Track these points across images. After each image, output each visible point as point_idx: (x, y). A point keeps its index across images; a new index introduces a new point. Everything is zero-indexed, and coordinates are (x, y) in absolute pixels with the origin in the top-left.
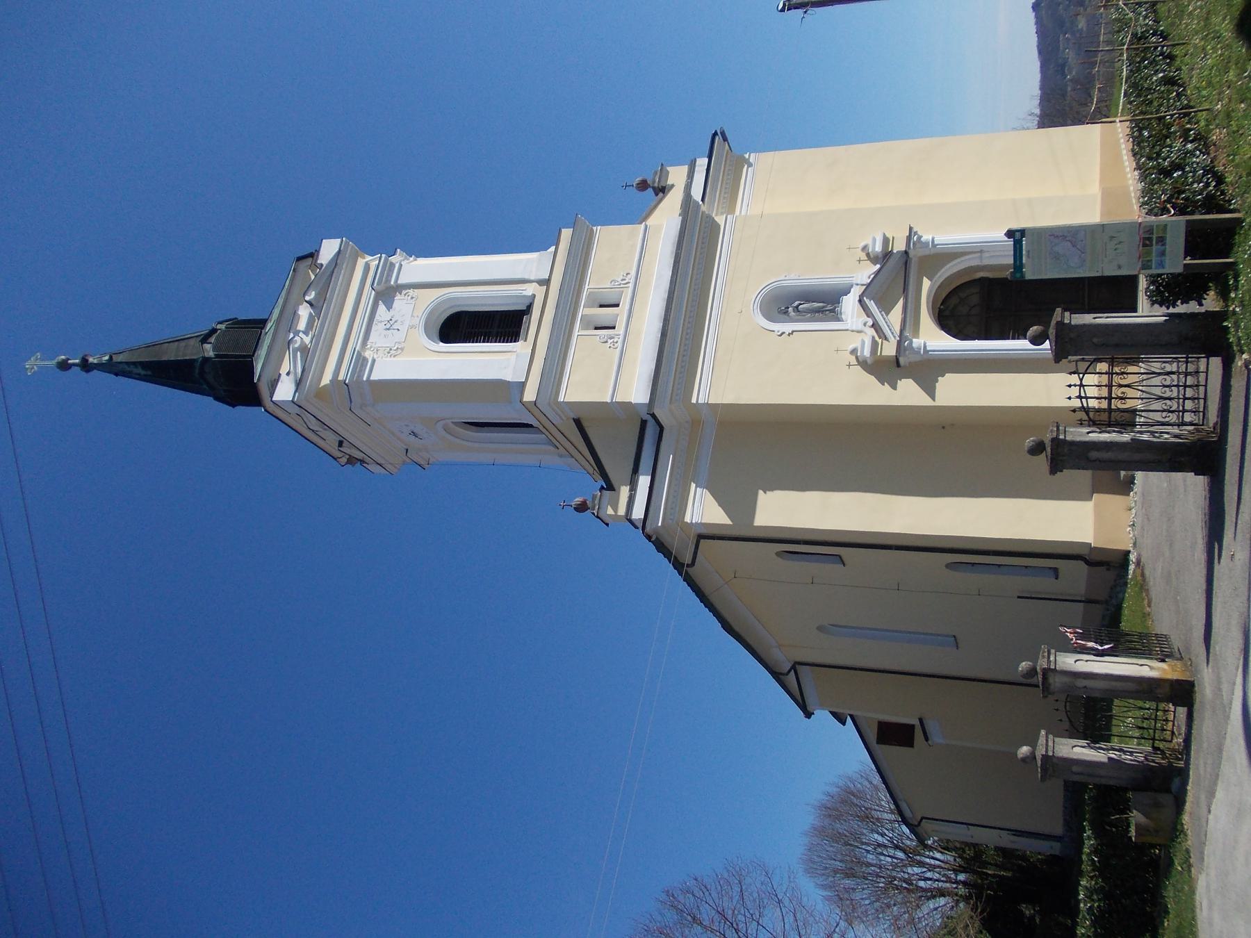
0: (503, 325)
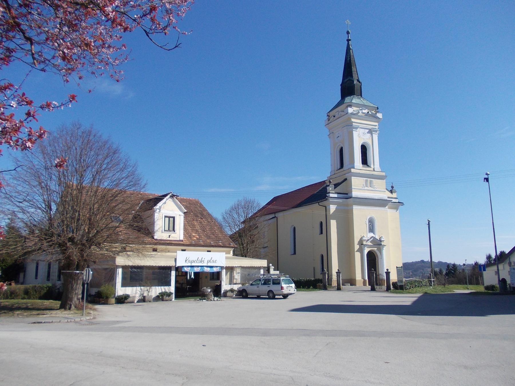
0: (365, 161)
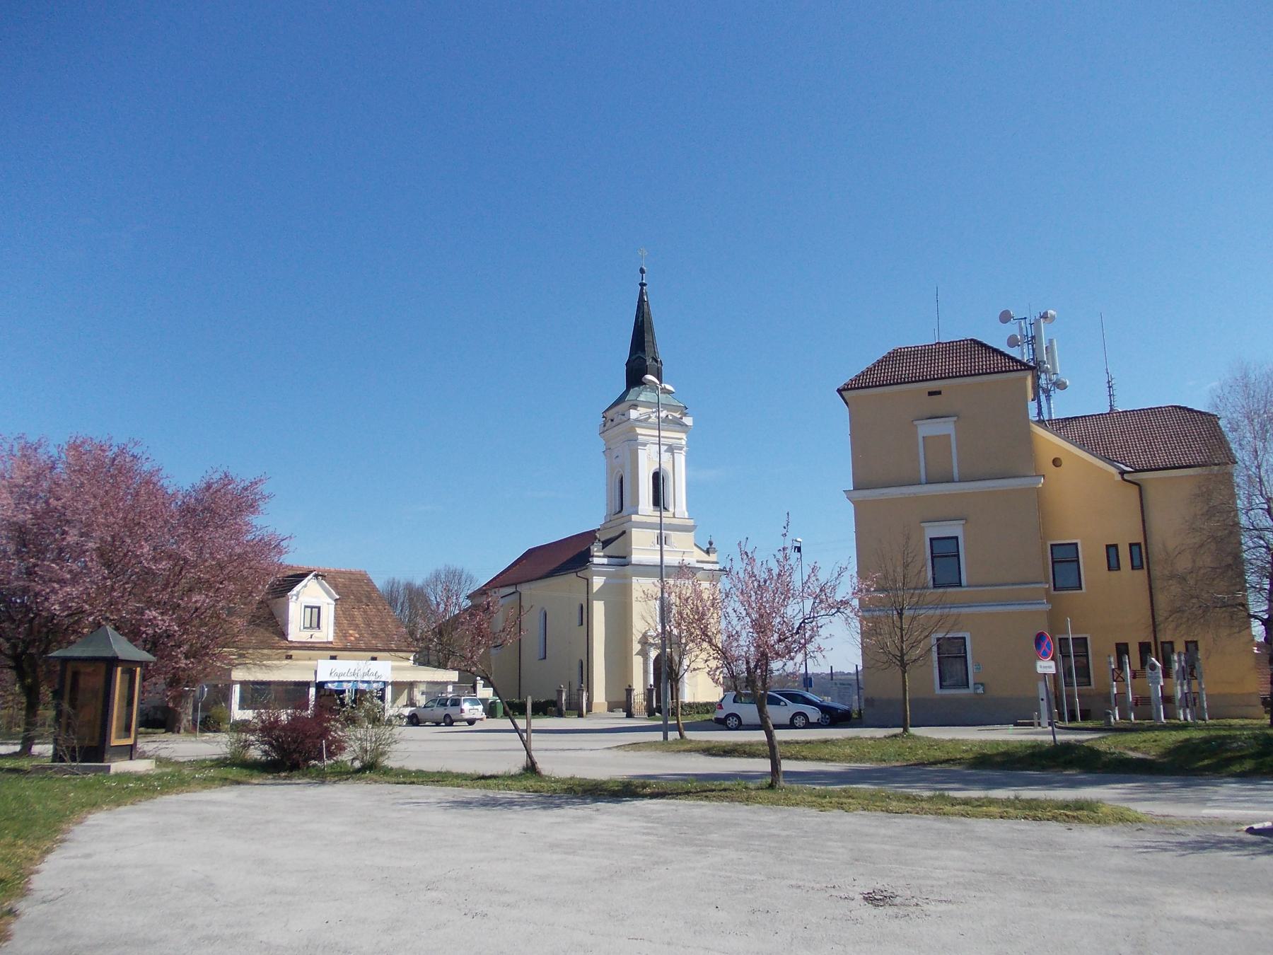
0: (658, 501)
